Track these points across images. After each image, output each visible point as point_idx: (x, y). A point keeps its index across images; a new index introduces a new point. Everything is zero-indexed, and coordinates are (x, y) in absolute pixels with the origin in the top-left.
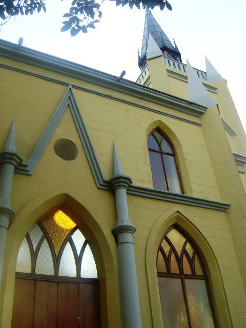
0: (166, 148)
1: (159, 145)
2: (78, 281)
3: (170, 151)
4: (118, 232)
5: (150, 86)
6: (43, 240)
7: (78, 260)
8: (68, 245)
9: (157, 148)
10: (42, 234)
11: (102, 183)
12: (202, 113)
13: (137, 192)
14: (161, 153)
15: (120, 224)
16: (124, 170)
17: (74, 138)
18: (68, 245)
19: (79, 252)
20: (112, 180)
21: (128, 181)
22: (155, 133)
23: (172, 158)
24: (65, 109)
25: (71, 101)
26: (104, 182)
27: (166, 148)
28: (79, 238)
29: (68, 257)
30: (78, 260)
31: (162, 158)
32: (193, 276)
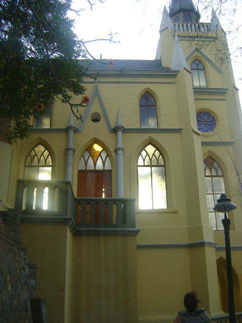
4: (116, 151)
12: (176, 75)
15: (69, 147)
16: (120, 123)
17: (99, 111)
20: (116, 127)
28: (47, 153)
29: (99, 163)
31: (117, 222)
32: (217, 176)
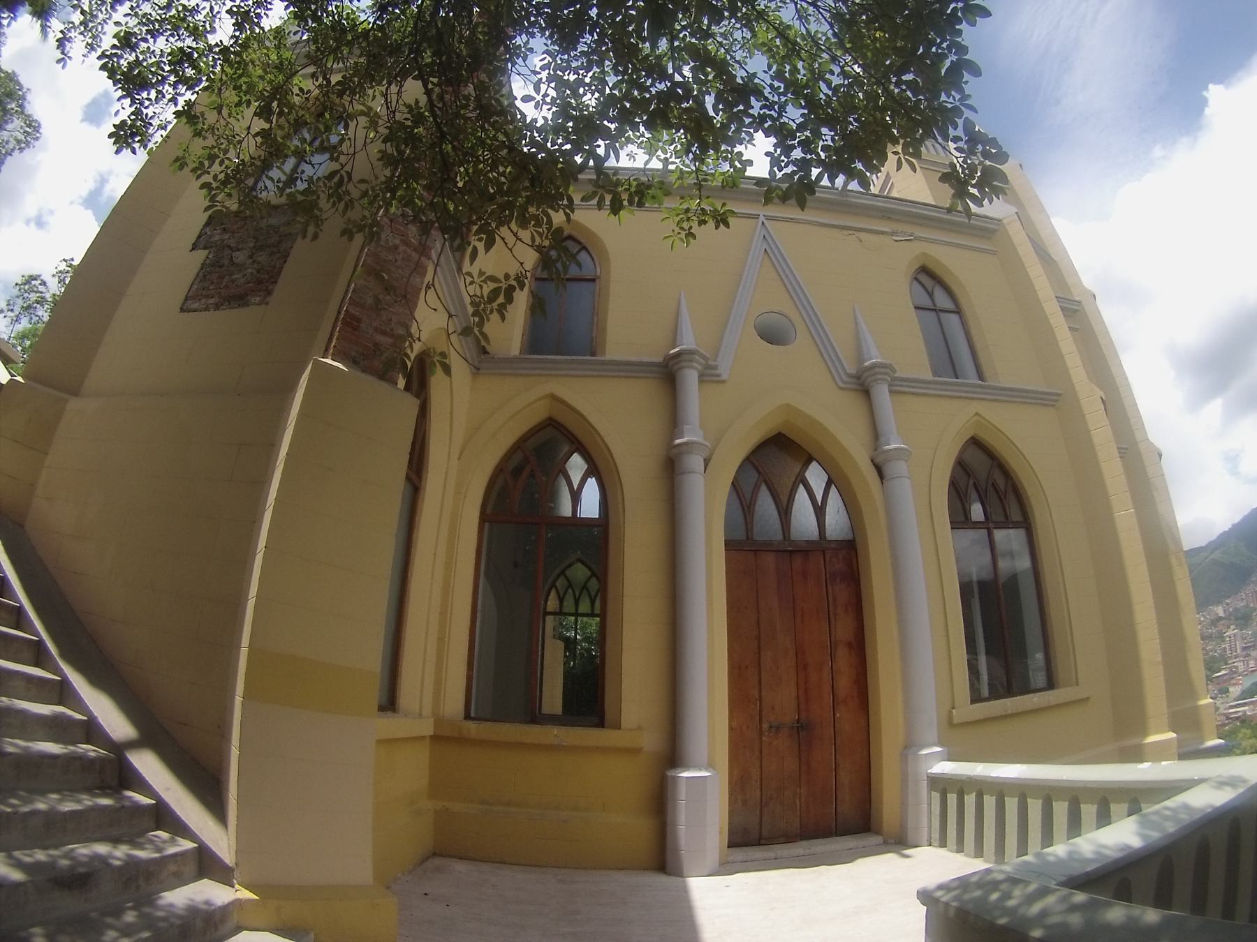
0: (942, 300)
1: (931, 295)
2: (576, 522)
3: (948, 304)
5: (894, 194)
6: (759, 487)
7: (820, 511)
8: (801, 490)
9: (926, 301)
10: (755, 475)
11: (845, 378)
13: (900, 387)
14: (936, 310)
18: (801, 490)
19: (819, 499)
21: (889, 370)
22: (918, 276)
23: (954, 318)
24: (760, 259)
25: (768, 243)
26: (850, 376)
27: (942, 300)
29: (802, 506)
30: (820, 511)
